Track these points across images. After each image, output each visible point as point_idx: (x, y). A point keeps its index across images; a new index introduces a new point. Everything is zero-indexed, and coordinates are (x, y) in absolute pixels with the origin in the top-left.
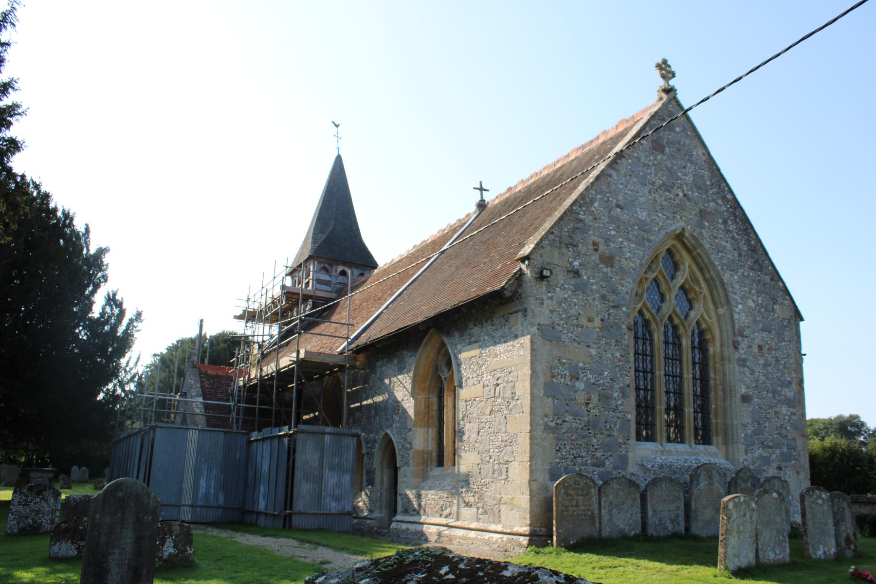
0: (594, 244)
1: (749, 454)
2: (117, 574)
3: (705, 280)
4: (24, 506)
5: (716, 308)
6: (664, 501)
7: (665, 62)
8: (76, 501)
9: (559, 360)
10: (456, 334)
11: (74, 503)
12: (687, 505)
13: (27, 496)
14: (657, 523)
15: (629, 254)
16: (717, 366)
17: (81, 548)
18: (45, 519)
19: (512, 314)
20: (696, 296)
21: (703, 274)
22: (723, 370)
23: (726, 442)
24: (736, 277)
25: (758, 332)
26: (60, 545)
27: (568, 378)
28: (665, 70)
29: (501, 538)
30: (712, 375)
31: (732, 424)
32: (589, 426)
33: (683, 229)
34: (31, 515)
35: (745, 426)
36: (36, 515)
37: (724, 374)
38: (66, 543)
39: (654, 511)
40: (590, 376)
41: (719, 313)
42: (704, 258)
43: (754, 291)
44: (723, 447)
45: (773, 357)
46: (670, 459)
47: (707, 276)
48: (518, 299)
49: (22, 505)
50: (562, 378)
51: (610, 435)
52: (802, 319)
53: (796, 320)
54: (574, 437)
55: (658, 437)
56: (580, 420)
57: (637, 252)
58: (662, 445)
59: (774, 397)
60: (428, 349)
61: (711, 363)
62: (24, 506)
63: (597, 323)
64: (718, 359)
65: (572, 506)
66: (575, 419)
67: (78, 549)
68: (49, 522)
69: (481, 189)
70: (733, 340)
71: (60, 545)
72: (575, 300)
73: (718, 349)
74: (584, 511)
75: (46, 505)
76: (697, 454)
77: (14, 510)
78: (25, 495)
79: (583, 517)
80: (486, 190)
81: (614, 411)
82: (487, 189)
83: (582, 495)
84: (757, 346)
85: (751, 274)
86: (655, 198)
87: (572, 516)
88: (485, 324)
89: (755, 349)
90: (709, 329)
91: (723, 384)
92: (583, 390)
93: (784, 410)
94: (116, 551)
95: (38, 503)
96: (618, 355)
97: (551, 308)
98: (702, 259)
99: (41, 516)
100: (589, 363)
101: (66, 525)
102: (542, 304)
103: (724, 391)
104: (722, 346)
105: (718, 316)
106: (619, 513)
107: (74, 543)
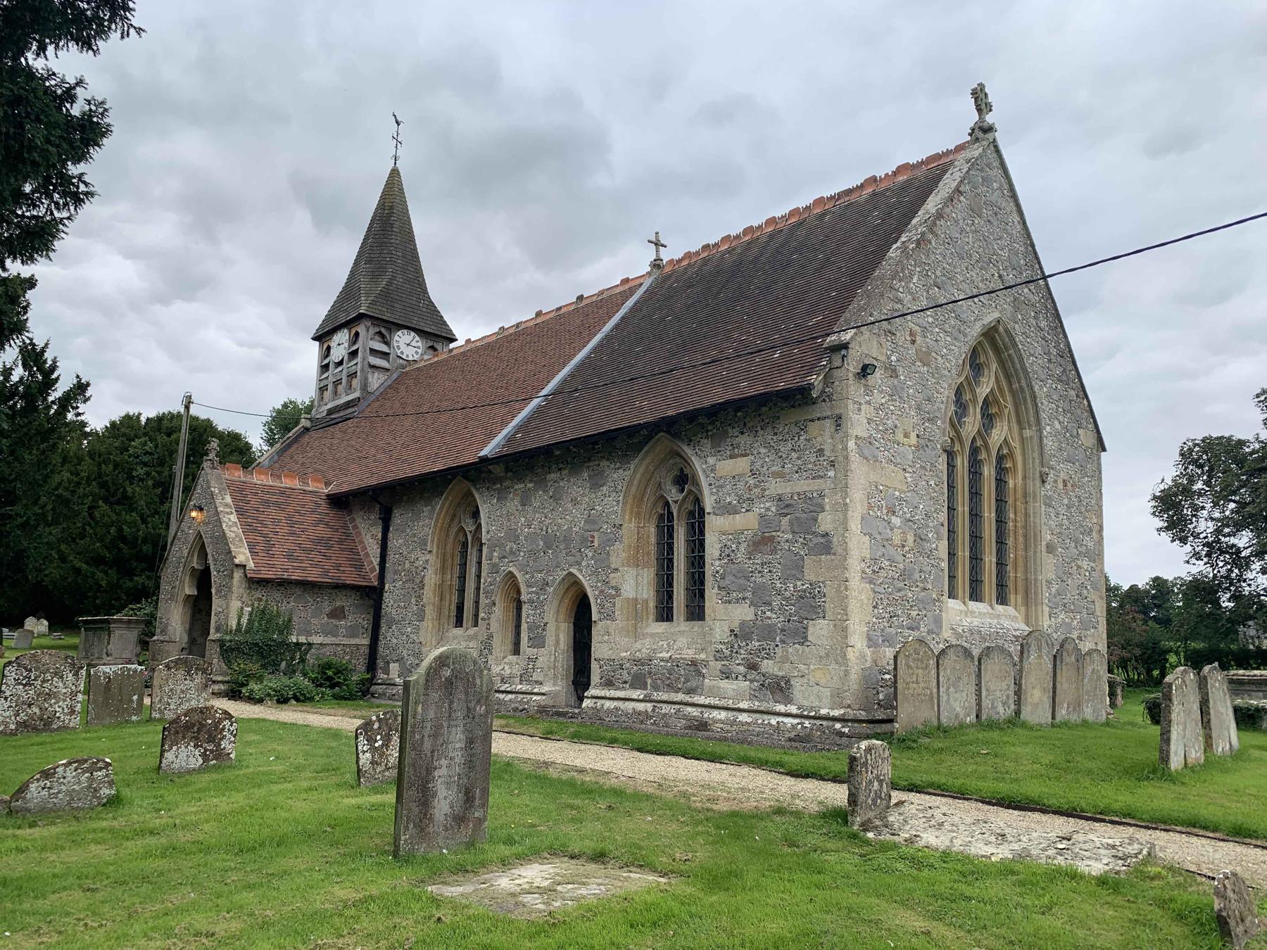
0: (912, 334)
1: (1053, 619)
2: (445, 798)
3: (1011, 390)
4: (25, 685)
5: (1021, 428)
6: (997, 677)
7: (982, 86)
8: (109, 678)
9: (876, 487)
10: (707, 444)
11: (104, 679)
12: (1018, 684)
13: (30, 671)
14: (990, 706)
15: (945, 350)
16: (1018, 503)
17: (208, 753)
18: (59, 707)
19: (812, 420)
20: (1000, 411)
21: (1010, 384)
22: (1026, 509)
23: (1027, 603)
24: (1045, 389)
25: (1063, 463)
26: (178, 749)
27: (885, 511)
28: (980, 99)
29: (802, 724)
30: (1012, 516)
31: (1036, 580)
32: (905, 575)
33: (999, 321)
34: (37, 700)
35: (1049, 582)
36: (45, 700)
37: (1026, 515)
38: (186, 747)
39: (988, 690)
40: (906, 509)
41: (1024, 436)
42: (1017, 361)
43: (1060, 410)
44: (1023, 609)
45: (1076, 497)
46: (976, 622)
47: (1016, 386)
48: (824, 401)
49: (20, 684)
50: (878, 510)
51: (925, 589)
52: (1104, 450)
53: (1098, 450)
54: (890, 590)
55: (960, 592)
56: (895, 566)
57: (953, 348)
58: (964, 603)
59: (1076, 547)
60: (648, 460)
61: (1011, 501)
62: (25, 685)
63: (913, 439)
64: (1019, 494)
65: (913, 683)
66: (891, 566)
67: (204, 755)
68: (66, 711)
69: (658, 244)
70: (1040, 472)
71: (178, 749)
72: (892, 407)
73: (1020, 481)
74: (923, 689)
75: (61, 685)
76: (998, 616)
77: (8, 693)
78: (25, 668)
79: (923, 698)
80: (663, 246)
81: (928, 557)
82: (665, 244)
83: (922, 668)
84: (1061, 480)
85: (1059, 387)
86: (972, 276)
87: (913, 695)
88: (761, 432)
89: (1061, 486)
90: (1011, 455)
91: (1025, 527)
92: (899, 528)
93: (1085, 564)
94: (444, 762)
95: (48, 680)
96: (932, 483)
97: (868, 416)
98: (1013, 363)
99: (53, 701)
100: (905, 492)
101: (187, 718)
102: (860, 410)
103: (1025, 536)
104: (1024, 478)
105: (1022, 440)
106: (956, 692)
107: (199, 746)
